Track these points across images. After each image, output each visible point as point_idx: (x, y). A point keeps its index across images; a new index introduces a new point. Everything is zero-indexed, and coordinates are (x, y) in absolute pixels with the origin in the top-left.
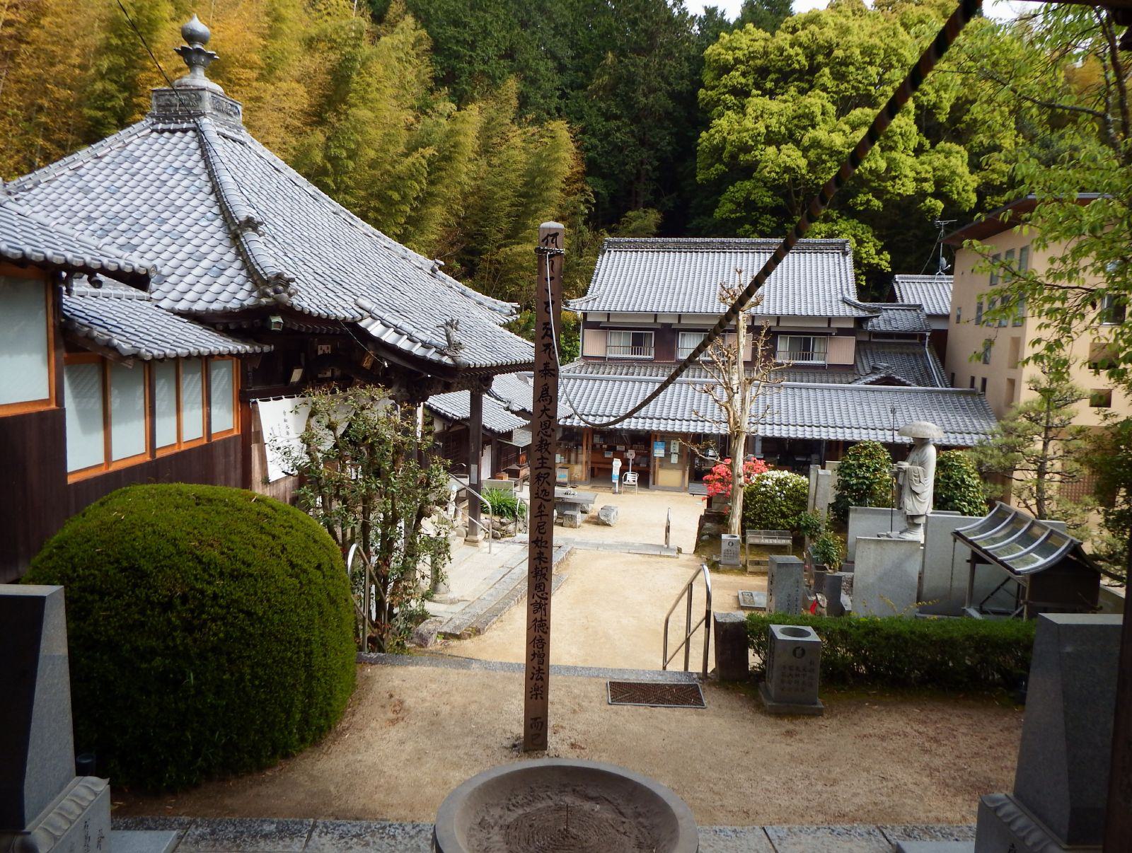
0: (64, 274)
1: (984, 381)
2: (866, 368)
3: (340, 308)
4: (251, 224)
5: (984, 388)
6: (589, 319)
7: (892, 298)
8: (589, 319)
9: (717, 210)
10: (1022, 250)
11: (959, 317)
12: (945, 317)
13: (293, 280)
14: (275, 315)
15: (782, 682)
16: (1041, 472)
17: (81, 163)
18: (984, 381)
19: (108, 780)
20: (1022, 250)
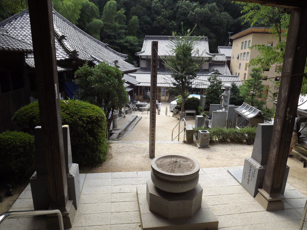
0: (25, 54)
1: (239, 74)
2: (211, 70)
3: (88, 58)
4: (63, 37)
5: (239, 75)
6: (142, 58)
7: (218, 52)
8: (142, 58)
9: (192, 51)
10: (245, 42)
11: (233, 57)
12: (230, 57)
13: (78, 52)
14: (73, 61)
15: (202, 142)
16: (15, 224)
17: (11, 20)
18: (239, 74)
19: (78, 164)
20: (245, 42)
